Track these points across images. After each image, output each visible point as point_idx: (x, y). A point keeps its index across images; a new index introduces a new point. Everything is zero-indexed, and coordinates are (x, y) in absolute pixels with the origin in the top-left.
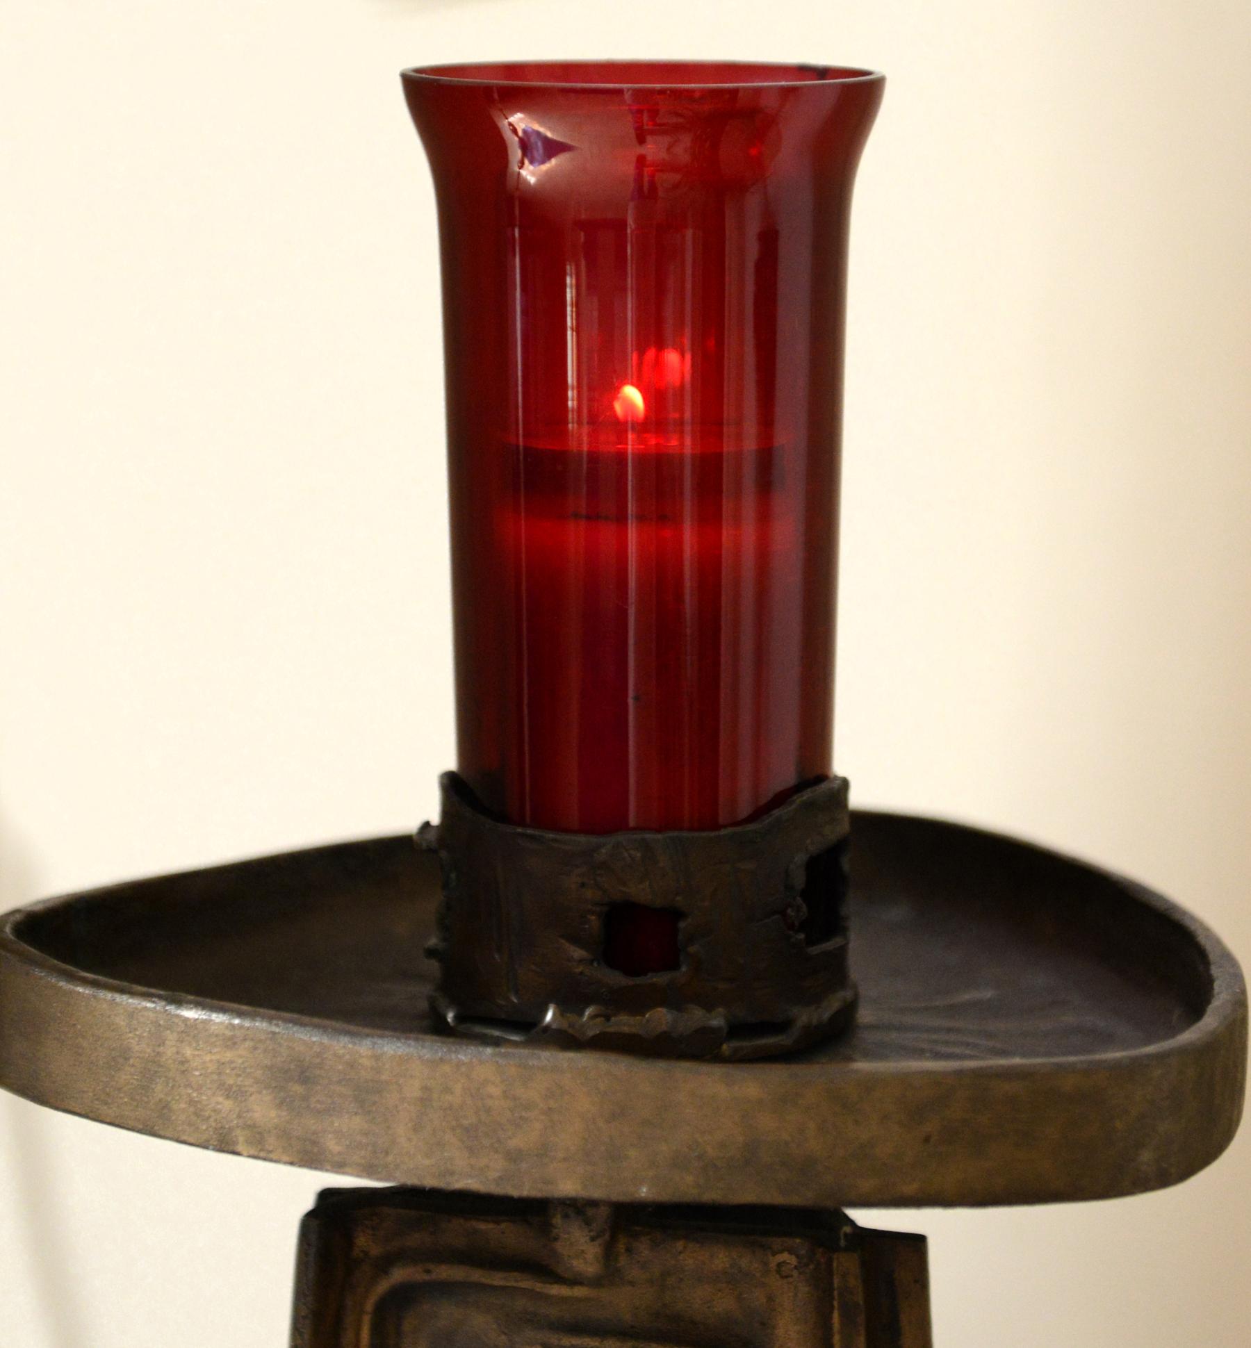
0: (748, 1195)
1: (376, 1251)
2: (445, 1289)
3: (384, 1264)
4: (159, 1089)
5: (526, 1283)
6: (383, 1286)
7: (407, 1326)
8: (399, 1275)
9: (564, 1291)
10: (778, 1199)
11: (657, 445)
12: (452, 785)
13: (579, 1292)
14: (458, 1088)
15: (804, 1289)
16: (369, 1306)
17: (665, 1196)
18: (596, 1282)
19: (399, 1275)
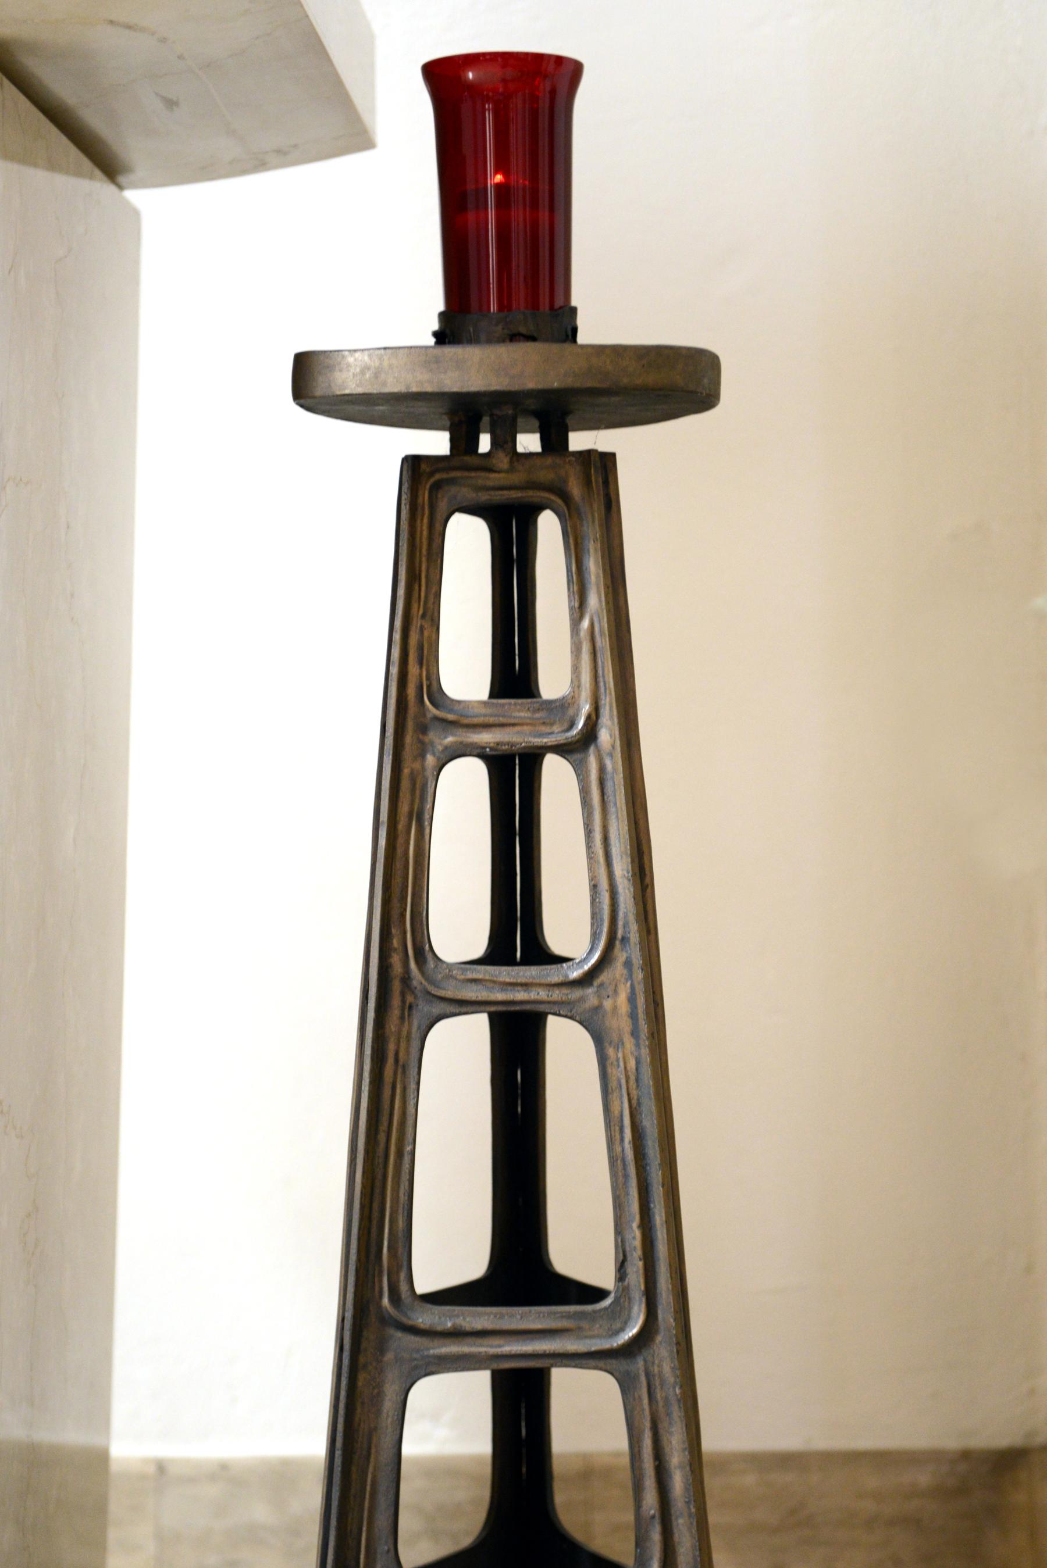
0: (589, 384)
1: (428, 470)
2: (452, 481)
3: (432, 474)
4: (383, 375)
5: (483, 474)
6: (432, 480)
7: (439, 496)
8: (438, 476)
9: (496, 475)
10: (598, 385)
11: (349, 365)
12: (442, 316)
13: (502, 475)
14: (493, 357)
15: (578, 468)
16: (428, 487)
17: (563, 385)
18: (507, 472)
19: (438, 476)
